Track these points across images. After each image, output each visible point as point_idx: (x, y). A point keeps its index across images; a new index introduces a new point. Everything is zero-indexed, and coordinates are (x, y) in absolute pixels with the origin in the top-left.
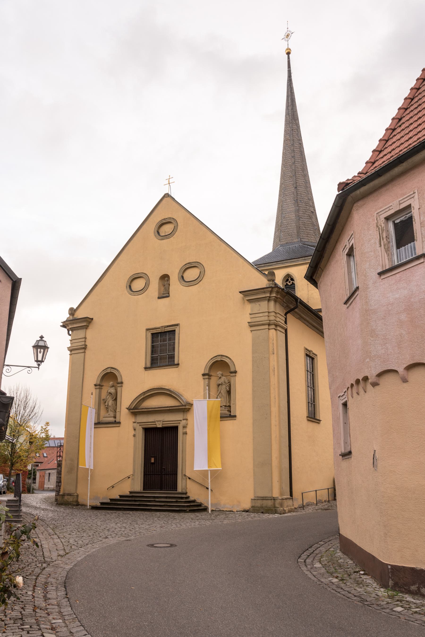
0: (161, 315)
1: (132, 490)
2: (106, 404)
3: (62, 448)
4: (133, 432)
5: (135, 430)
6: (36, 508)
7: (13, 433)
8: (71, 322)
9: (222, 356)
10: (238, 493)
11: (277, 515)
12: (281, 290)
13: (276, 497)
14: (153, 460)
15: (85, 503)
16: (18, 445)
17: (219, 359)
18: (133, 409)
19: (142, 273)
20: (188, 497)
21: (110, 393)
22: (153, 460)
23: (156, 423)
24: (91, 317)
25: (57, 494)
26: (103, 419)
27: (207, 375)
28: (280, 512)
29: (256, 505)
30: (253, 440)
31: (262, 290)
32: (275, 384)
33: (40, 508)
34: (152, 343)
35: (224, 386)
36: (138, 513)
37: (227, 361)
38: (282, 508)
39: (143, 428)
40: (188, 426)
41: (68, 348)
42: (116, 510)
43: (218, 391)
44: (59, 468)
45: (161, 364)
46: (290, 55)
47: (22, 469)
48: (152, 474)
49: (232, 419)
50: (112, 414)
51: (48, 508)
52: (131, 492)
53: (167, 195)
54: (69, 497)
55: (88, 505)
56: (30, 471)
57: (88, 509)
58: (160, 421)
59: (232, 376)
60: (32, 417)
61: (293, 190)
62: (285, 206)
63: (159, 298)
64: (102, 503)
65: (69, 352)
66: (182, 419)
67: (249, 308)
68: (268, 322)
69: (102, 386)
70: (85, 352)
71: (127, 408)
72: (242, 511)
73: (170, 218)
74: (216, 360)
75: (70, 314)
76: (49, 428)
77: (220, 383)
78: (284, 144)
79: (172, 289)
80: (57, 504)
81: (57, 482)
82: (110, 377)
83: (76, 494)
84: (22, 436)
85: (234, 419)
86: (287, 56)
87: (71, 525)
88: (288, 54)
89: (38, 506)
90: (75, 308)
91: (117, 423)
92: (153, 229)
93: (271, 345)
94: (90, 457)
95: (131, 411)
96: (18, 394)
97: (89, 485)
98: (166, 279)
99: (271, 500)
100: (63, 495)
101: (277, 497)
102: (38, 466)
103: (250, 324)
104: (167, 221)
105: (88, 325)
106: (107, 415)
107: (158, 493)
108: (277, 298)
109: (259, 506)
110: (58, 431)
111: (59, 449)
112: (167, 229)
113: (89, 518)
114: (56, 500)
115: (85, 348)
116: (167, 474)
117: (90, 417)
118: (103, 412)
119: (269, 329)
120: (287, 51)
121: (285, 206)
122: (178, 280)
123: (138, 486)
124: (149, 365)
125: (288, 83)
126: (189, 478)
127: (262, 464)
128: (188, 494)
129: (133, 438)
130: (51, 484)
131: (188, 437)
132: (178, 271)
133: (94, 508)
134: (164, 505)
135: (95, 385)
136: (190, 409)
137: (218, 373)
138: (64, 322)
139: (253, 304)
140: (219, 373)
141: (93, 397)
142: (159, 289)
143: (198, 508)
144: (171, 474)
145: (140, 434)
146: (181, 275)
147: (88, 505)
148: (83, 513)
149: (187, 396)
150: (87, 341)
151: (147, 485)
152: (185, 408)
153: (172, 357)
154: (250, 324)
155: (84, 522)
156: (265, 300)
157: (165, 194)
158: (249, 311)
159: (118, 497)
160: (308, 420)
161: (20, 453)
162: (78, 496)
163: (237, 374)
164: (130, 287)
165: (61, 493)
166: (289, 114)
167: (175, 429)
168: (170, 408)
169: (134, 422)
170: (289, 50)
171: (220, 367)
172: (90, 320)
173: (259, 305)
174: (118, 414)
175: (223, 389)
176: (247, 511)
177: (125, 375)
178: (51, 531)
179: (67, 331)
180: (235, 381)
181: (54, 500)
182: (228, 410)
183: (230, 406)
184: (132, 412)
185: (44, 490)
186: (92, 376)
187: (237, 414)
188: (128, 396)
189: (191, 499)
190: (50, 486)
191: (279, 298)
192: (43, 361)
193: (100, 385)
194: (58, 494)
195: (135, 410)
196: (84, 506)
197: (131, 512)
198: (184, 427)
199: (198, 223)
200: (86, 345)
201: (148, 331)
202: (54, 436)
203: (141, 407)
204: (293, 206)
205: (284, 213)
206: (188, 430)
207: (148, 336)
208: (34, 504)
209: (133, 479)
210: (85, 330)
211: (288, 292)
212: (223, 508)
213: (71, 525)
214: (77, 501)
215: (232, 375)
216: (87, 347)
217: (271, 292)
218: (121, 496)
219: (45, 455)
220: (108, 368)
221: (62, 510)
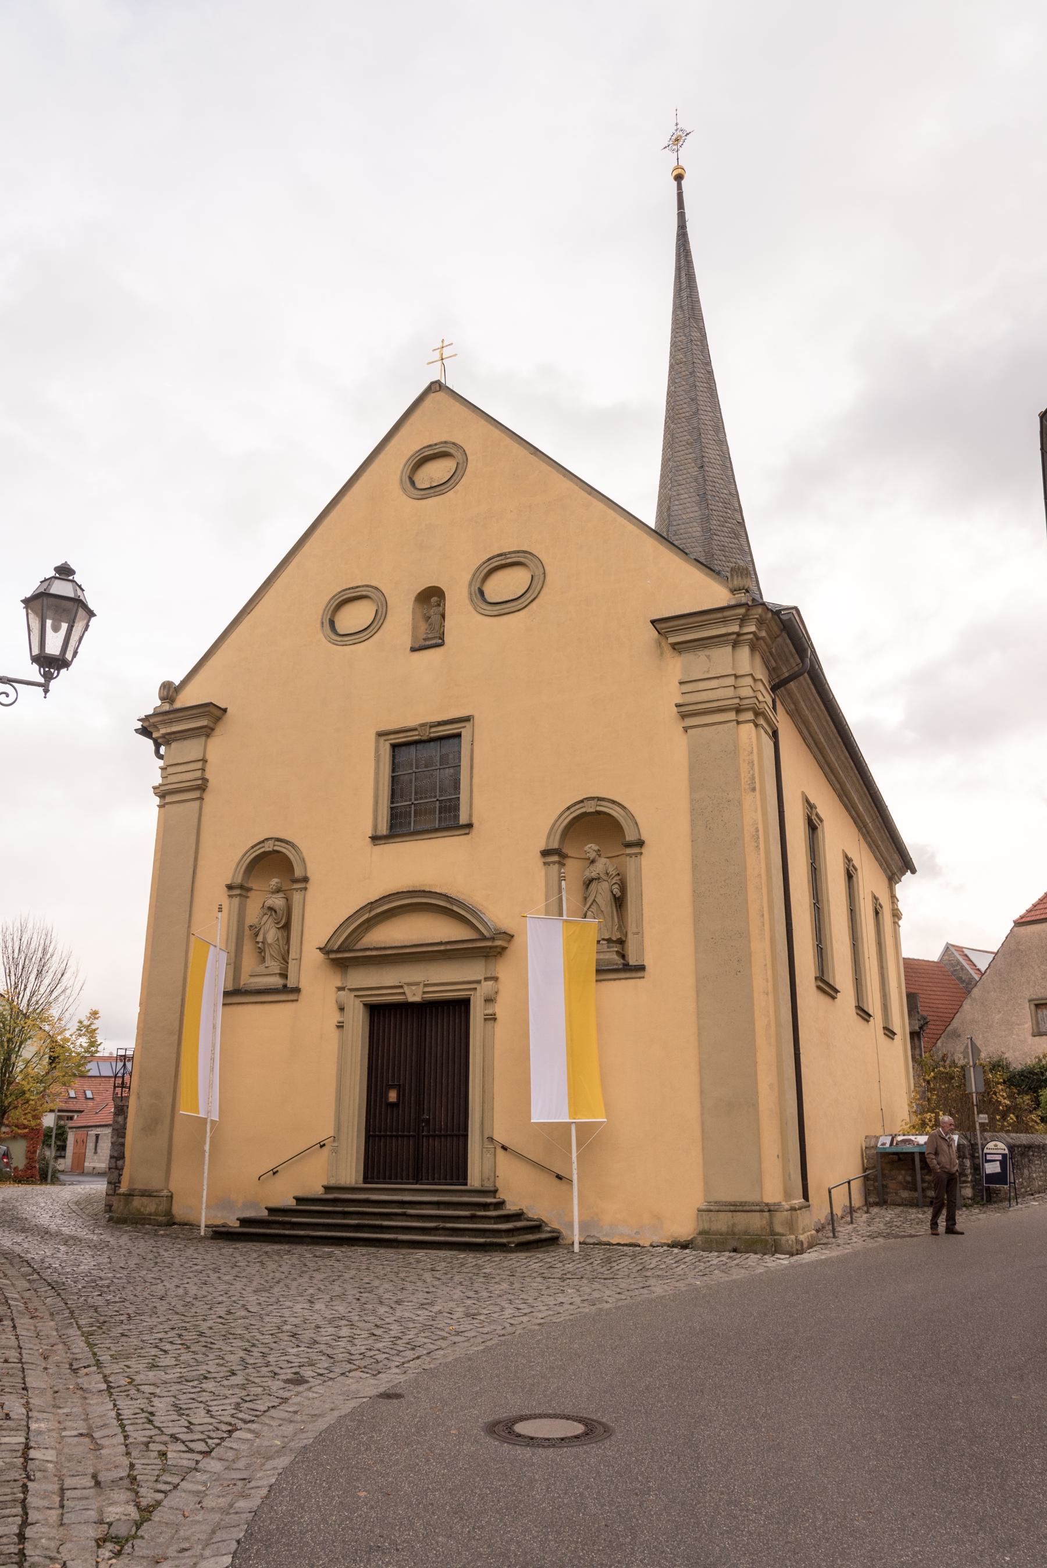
0: (416, 691)
1: (332, 1182)
2: (260, 938)
3: (129, 1065)
4: (336, 1017)
5: (342, 1009)
6: (45, 1234)
7: (8, 1035)
8: (166, 717)
9: (599, 799)
10: (650, 1187)
11: (784, 1260)
12: (770, 615)
13: (775, 1204)
14: (393, 1096)
15: (191, 1218)
16: (20, 1065)
17: (590, 808)
18: (338, 951)
19: (367, 586)
20: (500, 1204)
21: (270, 908)
22: (393, 1096)
23: (406, 989)
24: (223, 706)
25: (111, 1192)
26: (246, 981)
27: (553, 854)
28: (789, 1249)
29: (714, 1227)
30: (699, 1034)
31: (719, 615)
32: (760, 875)
33: (58, 1234)
34: (393, 771)
35: (605, 885)
36: (360, 1252)
37: (615, 812)
38: (793, 1237)
39: (365, 1005)
40: (499, 999)
41: (154, 788)
42: (287, 1243)
43: (585, 899)
44: (120, 1119)
45: (419, 828)
46: (683, 182)
47: (26, 1122)
48: (391, 1136)
49: (634, 975)
50: (275, 966)
51: (83, 1233)
52: (328, 1189)
53: (436, 387)
54: (145, 1200)
55: (203, 1225)
56: (50, 1129)
57: (201, 1239)
58: (417, 984)
59: (630, 855)
60: (57, 997)
61: (694, 471)
62: (676, 508)
63: (413, 650)
64: (244, 1222)
65: (157, 800)
66: (481, 978)
67: (676, 667)
68: (737, 701)
69: (249, 890)
70: (201, 799)
71: (320, 949)
72: (669, 1246)
73: (446, 442)
74: (583, 810)
75: (162, 699)
76: (97, 1024)
77: (594, 875)
78: (670, 372)
79: (452, 625)
80: (110, 1219)
81: (112, 1157)
82: (273, 865)
83: (165, 1193)
84: (29, 1042)
85: (639, 974)
86: (676, 183)
87: (154, 1312)
88: (679, 178)
89: (53, 1228)
90: (177, 683)
91: (289, 991)
92: (399, 473)
93: (744, 768)
94: (211, 1085)
95: (333, 956)
96: (25, 940)
97: (206, 1167)
98: (434, 599)
99: (762, 1211)
100: (130, 1195)
101: (779, 1204)
102: (71, 1118)
103: (683, 709)
104: (436, 445)
105: (211, 725)
106: (261, 969)
107: (408, 1192)
108: (758, 638)
109: (724, 1229)
110: (119, 1037)
111: (120, 1064)
112: (437, 471)
113: (214, 1277)
114: (109, 1208)
115: (202, 786)
116: (434, 1136)
117: (213, 974)
118: (249, 961)
119: (738, 723)
120: (675, 173)
121: (676, 508)
122: (467, 601)
123: (349, 1171)
124: (383, 829)
125: (678, 240)
126: (504, 1148)
127: (726, 1105)
128: (502, 1195)
129: (334, 1034)
130: (99, 1160)
131: (500, 1030)
132: (469, 577)
133: (221, 1235)
134: (436, 1229)
135: (230, 887)
136: (504, 949)
137: (586, 848)
138: (147, 717)
139: (688, 657)
140: (591, 848)
141: (223, 917)
142: (415, 629)
143: (534, 1237)
144: (446, 1136)
145: (357, 1020)
146: (478, 585)
147: (203, 1225)
148: (190, 1252)
149: (497, 913)
150: (208, 768)
151: (374, 1167)
152: (490, 947)
153: (450, 808)
154: (683, 709)
155: (200, 1294)
156: (726, 642)
157: (432, 383)
158: (679, 676)
159: (291, 1203)
160: (819, 988)
161: (23, 1082)
162: (171, 1197)
163: (643, 850)
164: (332, 623)
165: (123, 1189)
166: (681, 307)
167: (462, 1006)
168: (449, 947)
169: (340, 989)
170: (680, 171)
171: (595, 831)
172: (218, 713)
173: (708, 657)
174: (292, 965)
175: (602, 893)
176: (684, 1246)
177: (314, 858)
178: (79, 1346)
179: (153, 747)
180: (639, 870)
181: (102, 1206)
182: (617, 952)
183: (621, 942)
184: (333, 960)
185: (83, 1173)
186: (221, 863)
187: (648, 962)
188: (321, 917)
189: (511, 1208)
190: (97, 1165)
191: (763, 638)
192: (66, 664)
193: (241, 887)
194: (114, 1184)
195: (344, 955)
196: (190, 1226)
197: (337, 1251)
198: (489, 1000)
199: (524, 452)
200: (205, 780)
201: (382, 739)
202: (111, 1053)
203: (357, 947)
204: (697, 509)
205: (675, 523)
206: (499, 1008)
207: (382, 752)
208: (44, 1219)
209: (335, 1151)
210: (203, 738)
211: (790, 620)
212: (606, 1235)
213: (154, 1312)
214: (169, 1213)
215: (629, 851)
216: (209, 784)
217: (743, 621)
218: (299, 1200)
219: (89, 1094)
220: (267, 839)
221: (124, 1240)
